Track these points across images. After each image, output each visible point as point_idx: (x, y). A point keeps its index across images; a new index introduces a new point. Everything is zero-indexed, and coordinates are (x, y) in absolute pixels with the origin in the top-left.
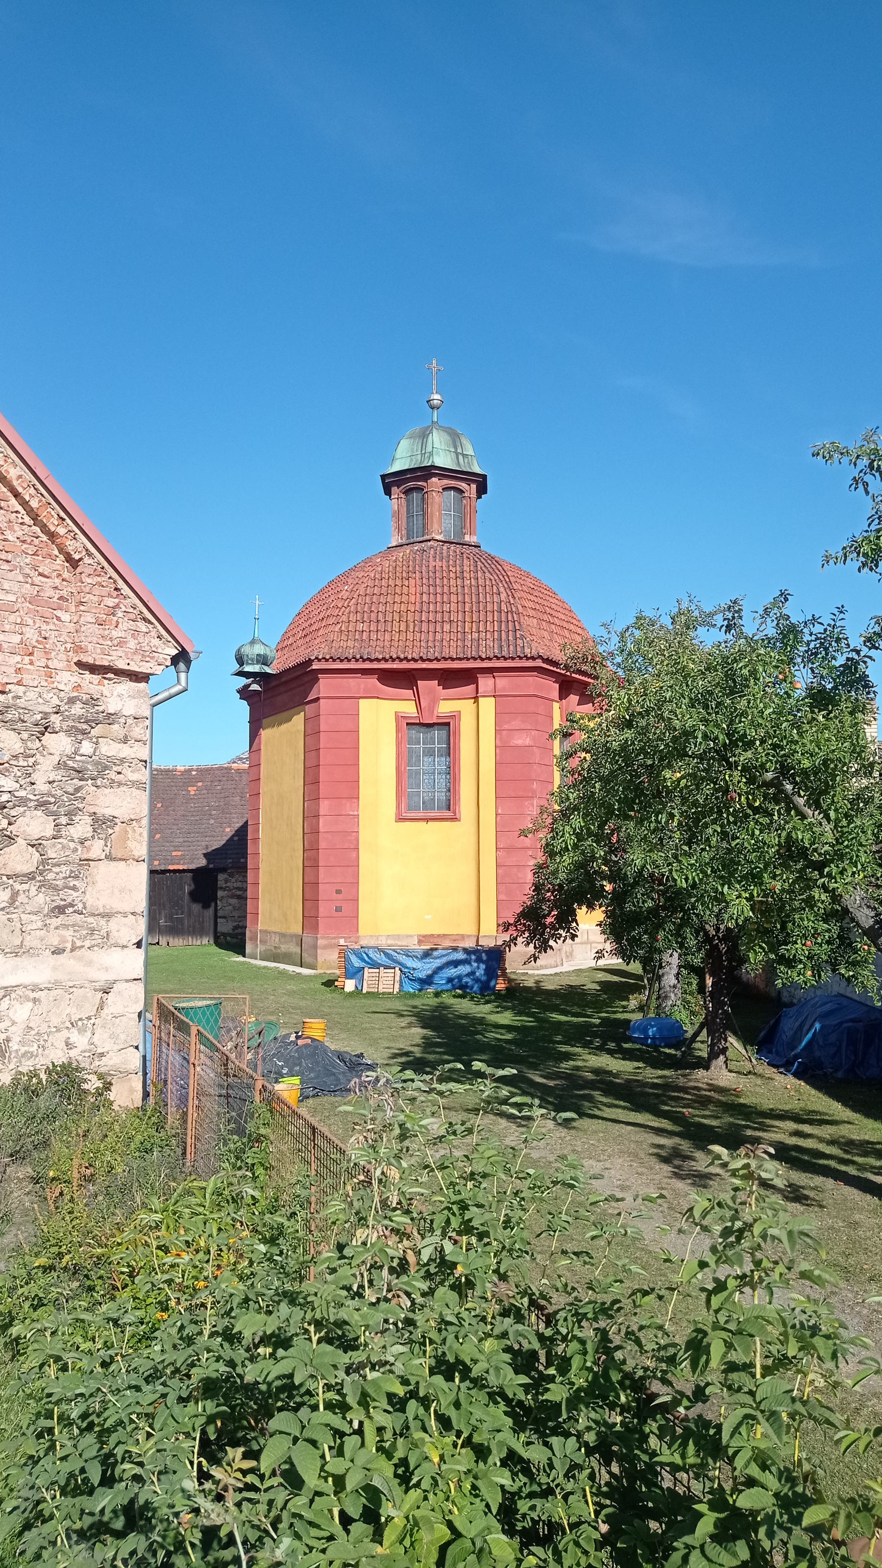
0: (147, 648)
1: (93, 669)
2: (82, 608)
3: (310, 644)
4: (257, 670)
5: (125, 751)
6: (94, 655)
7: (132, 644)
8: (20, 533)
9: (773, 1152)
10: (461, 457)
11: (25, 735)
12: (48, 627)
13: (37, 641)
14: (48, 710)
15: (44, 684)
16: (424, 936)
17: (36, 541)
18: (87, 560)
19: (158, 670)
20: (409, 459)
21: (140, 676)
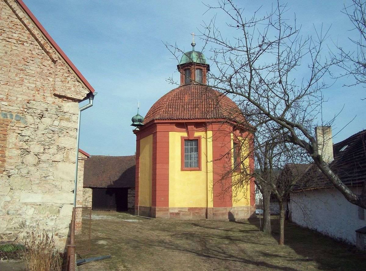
0: (78, 91)
1: (60, 97)
2: (56, 76)
4: (138, 124)
5: (70, 125)
6: (60, 92)
7: (73, 89)
10: (201, 60)
15: (43, 101)
16: (190, 208)
18: (59, 61)
21: (76, 100)
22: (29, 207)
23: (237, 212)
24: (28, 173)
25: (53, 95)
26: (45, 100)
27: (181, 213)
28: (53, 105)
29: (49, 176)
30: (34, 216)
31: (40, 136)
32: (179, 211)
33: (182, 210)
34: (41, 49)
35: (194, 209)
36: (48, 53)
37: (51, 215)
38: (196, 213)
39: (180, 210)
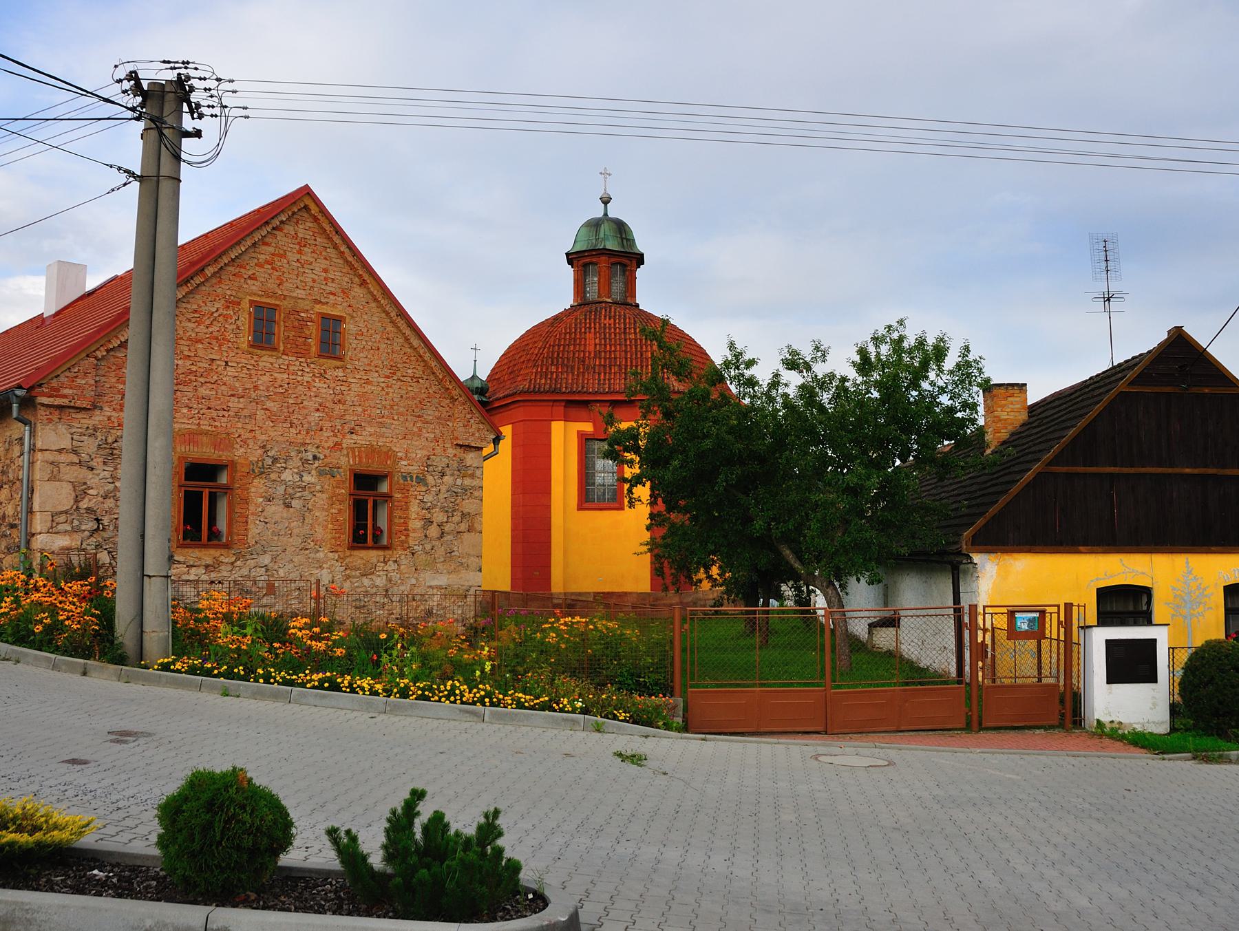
7: (477, 435)
9: (185, 104)
10: (625, 241)
14: (444, 465)
31: (444, 500)
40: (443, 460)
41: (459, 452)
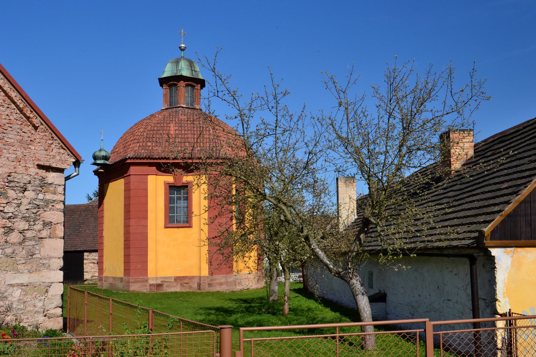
3: (126, 151)
7: (58, 158)
8: (15, 117)
10: (194, 72)
11: (17, 192)
12: (26, 152)
13: (22, 157)
15: (25, 173)
16: (177, 277)
17: (22, 120)
19: (68, 167)
20: (171, 72)
22: (15, 288)
23: (239, 281)
24: (13, 253)
25: (37, 165)
26: (28, 172)
27: (165, 284)
28: (36, 176)
29: (36, 254)
30: (21, 298)
31: (25, 211)
32: (162, 282)
33: (166, 280)
34: (20, 113)
35: (182, 279)
36: (28, 118)
37: (39, 296)
38: (186, 283)
39: (163, 280)
40: (26, 177)
41: (42, 172)
